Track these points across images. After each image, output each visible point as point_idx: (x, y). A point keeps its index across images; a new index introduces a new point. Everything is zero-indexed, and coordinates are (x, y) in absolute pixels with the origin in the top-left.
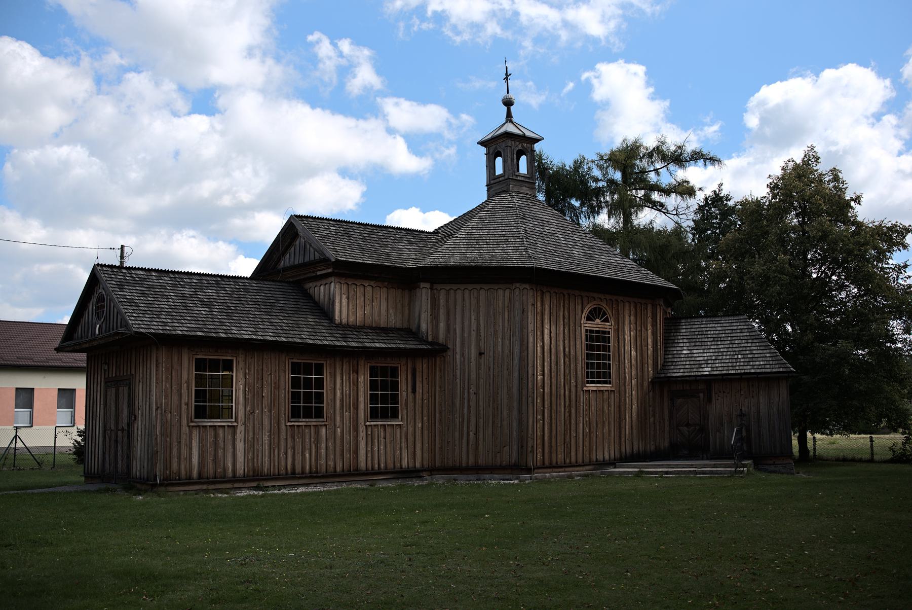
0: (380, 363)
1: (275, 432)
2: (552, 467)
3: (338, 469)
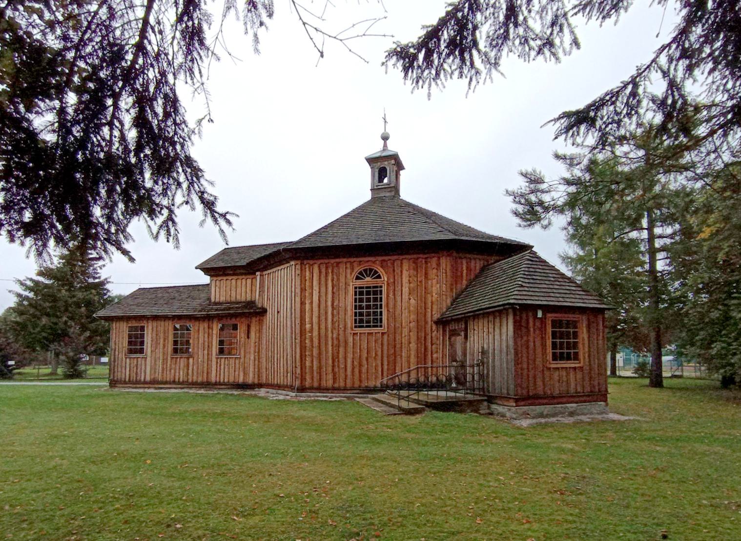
0: (134, 324)
1: (165, 360)
2: (320, 389)
3: (181, 380)
